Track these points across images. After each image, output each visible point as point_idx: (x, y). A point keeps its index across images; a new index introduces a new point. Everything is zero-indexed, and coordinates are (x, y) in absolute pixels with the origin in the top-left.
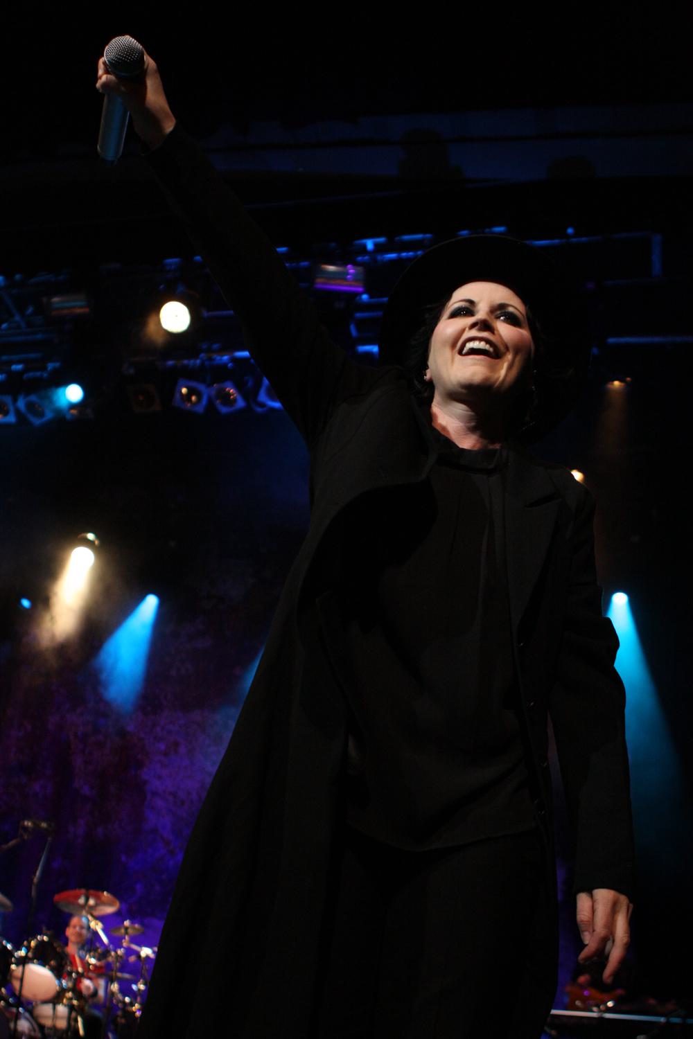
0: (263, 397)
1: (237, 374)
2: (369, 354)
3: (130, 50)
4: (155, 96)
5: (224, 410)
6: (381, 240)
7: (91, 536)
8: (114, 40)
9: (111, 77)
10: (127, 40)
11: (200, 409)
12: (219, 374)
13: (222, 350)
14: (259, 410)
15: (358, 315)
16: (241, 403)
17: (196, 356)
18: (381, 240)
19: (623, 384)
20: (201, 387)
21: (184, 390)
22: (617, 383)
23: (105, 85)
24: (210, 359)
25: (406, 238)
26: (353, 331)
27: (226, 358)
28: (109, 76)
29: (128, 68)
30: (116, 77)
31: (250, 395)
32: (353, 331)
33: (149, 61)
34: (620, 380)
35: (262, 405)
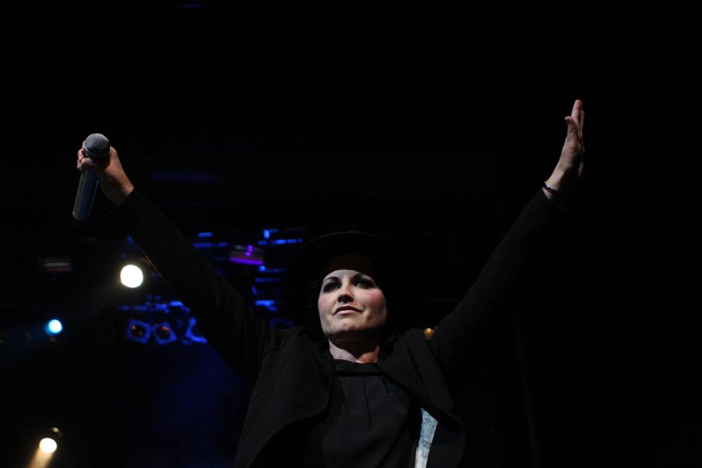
0: (189, 334)
1: (174, 317)
2: (263, 307)
3: (102, 142)
4: (114, 167)
5: (161, 342)
6: (275, 230)
7: (56, 430)
8: (89, 136)
9: (88, 159)
10: (99, 136)
11: (144, 340)
12: (159, 317)
13: (161, 302)
14: (186, 342)
15: (259, 280)
16: (173, 337)
17: (143, 305)
18: (275, 230)
19: (433, 331)
20: (146, 325)
21: (134, 327)
22: (429, 330)
23: (85, 165)
24: (153, 306)
25: (581, 166)
26: (254, 290)
27: (164, 306)
28: (87, 159)
29: (99, 155)
30: (91, 159)
31: (180, 332)
32: (254, 290)
33: (113, 150)
34: (432, 328)
35: (189, 339)
